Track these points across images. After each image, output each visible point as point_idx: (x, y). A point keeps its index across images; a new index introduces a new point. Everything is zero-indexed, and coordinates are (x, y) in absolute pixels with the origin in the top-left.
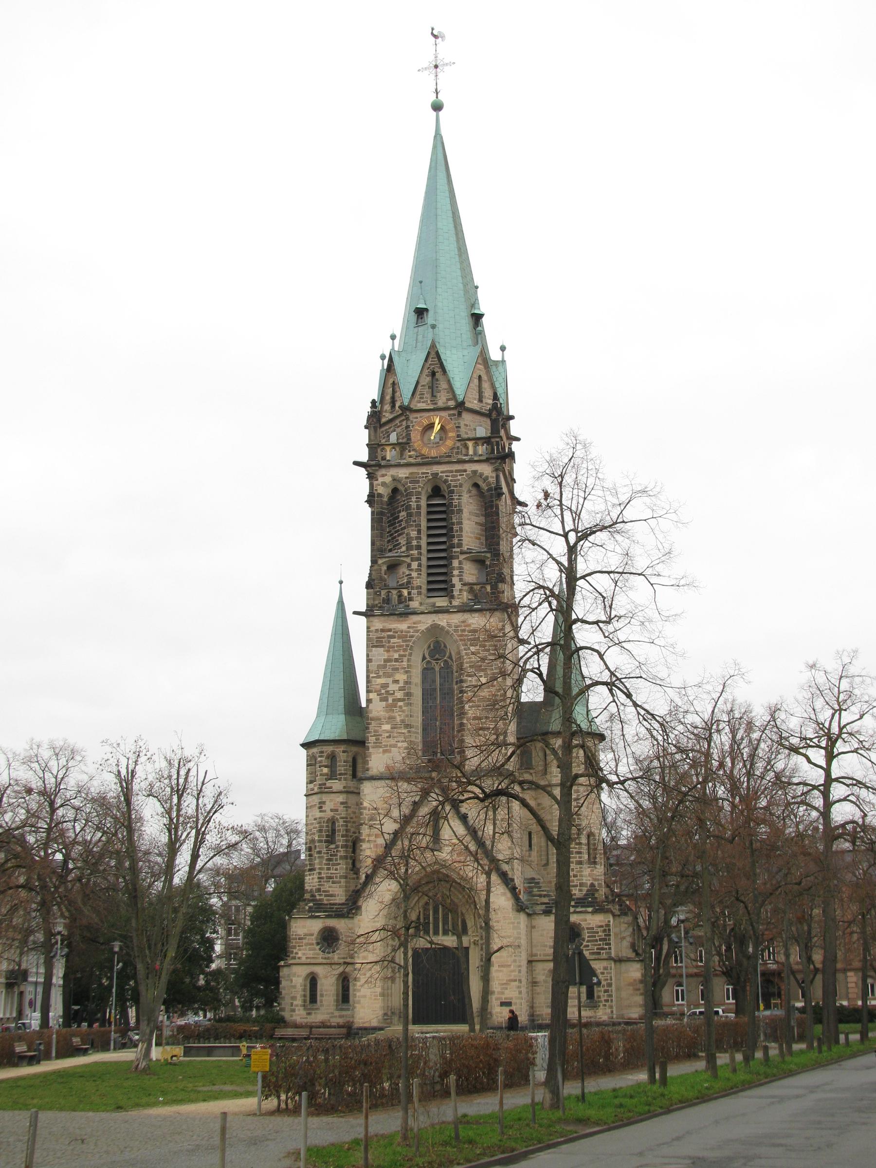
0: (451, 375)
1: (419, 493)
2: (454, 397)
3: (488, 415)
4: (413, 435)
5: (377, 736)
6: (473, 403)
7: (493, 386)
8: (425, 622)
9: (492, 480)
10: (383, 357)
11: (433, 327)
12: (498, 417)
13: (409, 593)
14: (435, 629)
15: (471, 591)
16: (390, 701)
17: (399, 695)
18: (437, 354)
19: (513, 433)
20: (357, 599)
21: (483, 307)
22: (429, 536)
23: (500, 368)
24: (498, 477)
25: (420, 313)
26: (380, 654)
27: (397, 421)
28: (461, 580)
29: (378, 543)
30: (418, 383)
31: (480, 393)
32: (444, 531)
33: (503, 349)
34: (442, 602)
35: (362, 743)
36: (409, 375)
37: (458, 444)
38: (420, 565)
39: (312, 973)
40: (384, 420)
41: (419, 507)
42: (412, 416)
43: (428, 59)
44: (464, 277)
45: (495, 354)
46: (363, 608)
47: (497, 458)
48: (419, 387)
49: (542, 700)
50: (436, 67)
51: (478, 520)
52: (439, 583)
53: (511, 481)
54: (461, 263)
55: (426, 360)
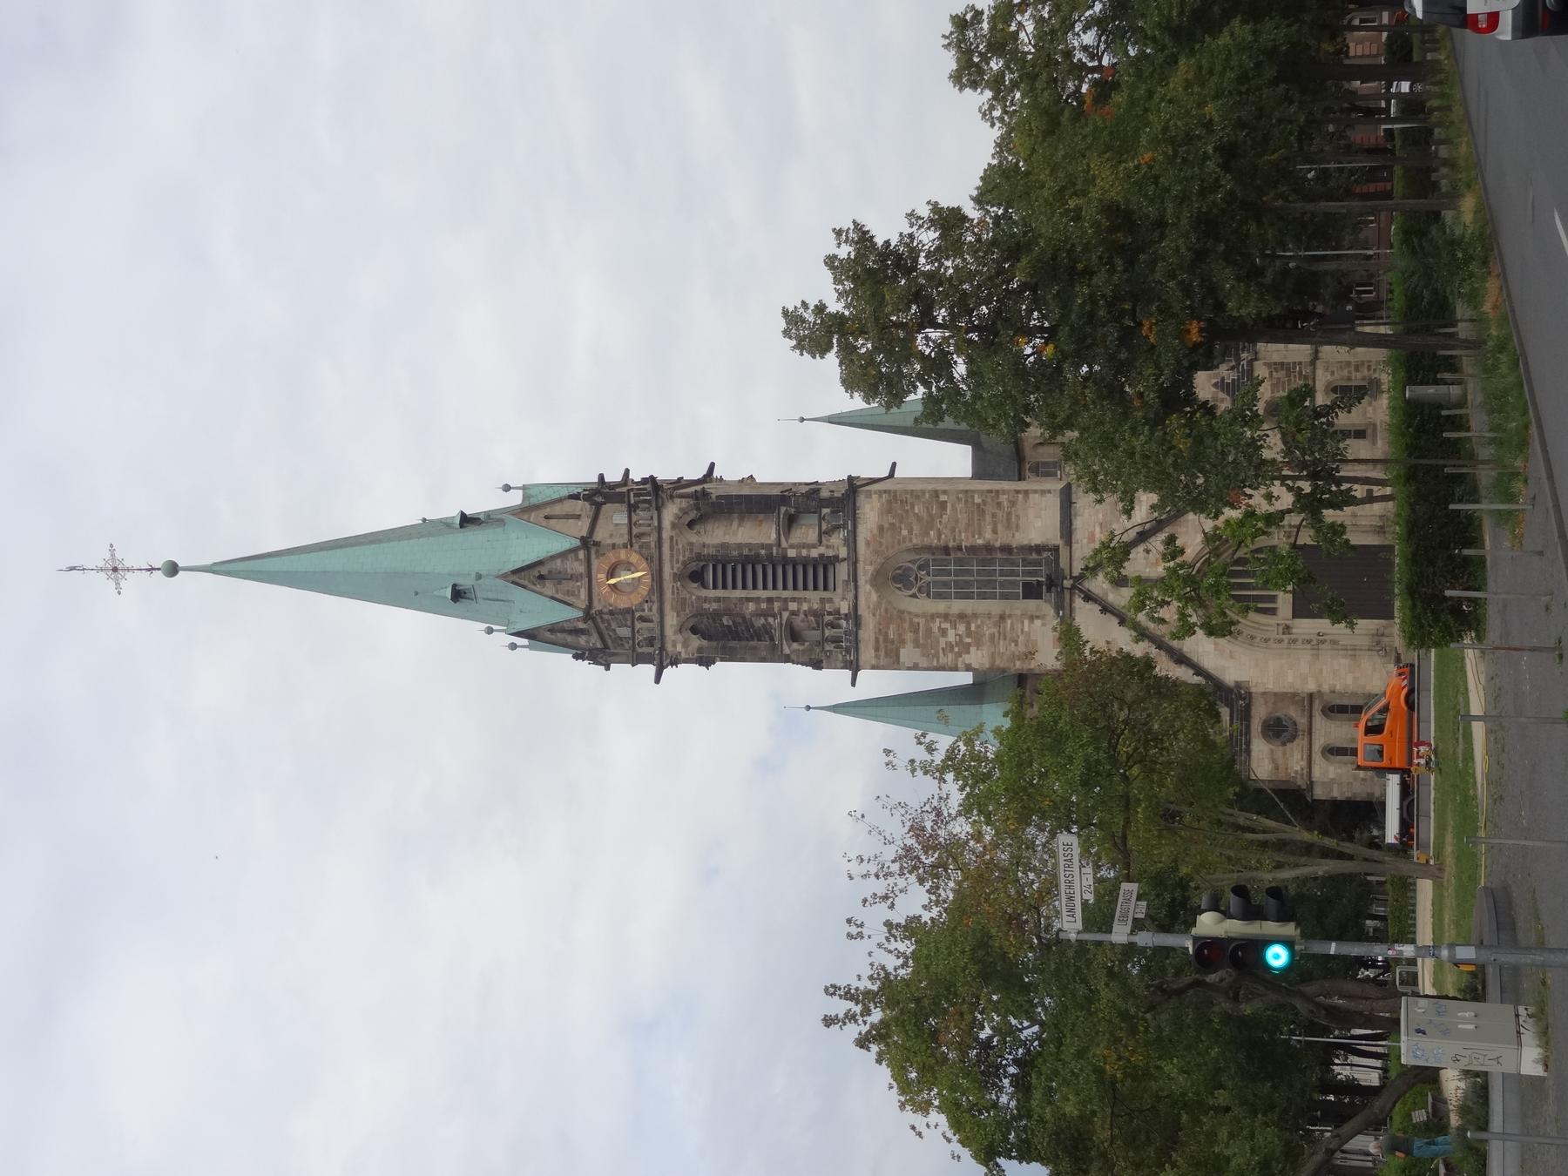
0: (543, 555)
1: (698, 598)
2: (574, 551)
3: (598, 507)
4: (622, 606)
5: (1013, 657)
6: (582, 528)
7: (560, 500)
8: (868, 595)
9: (684, 503)
10: (513, 646)
11: (479, 577)
12: (601, 495)
13: (830, 613)
14: (878, 580)
15: (828, 533)
16: (968, 640)
17: (962, 628)
18: (515, 572)
19: (618, 478)
20: (832, 683)
21: (451, 512)
22: (755, 587)
23: (532, 492)
24: (682, 496)
25: (458, 594)
26: (908, 653)
27: (602, 626)
28: (814, 546)
29: (764, 654)
30: (553, 598)
31: (568, 517)
32: (749, 568)
33: (507, 488)
34: (842, 571)
35: (1022, 679)
36: (543, 610)
37: (636, 547)
38: (794, 599)
39: (1323, 753)
40: (599, 645)
41: (718, 600)
42: (597, 606)
43: (103, 582)
44: (410, 537)
45: (515, 499)
46: (848, 673)
47: (657, 495)
48: (559, 596)
49: (969, 448)
50: (115, 570)
51: (735, 523)
52: (818, 571)
53: (679, 483)
54: (390, 540)
55: (524, 587)
